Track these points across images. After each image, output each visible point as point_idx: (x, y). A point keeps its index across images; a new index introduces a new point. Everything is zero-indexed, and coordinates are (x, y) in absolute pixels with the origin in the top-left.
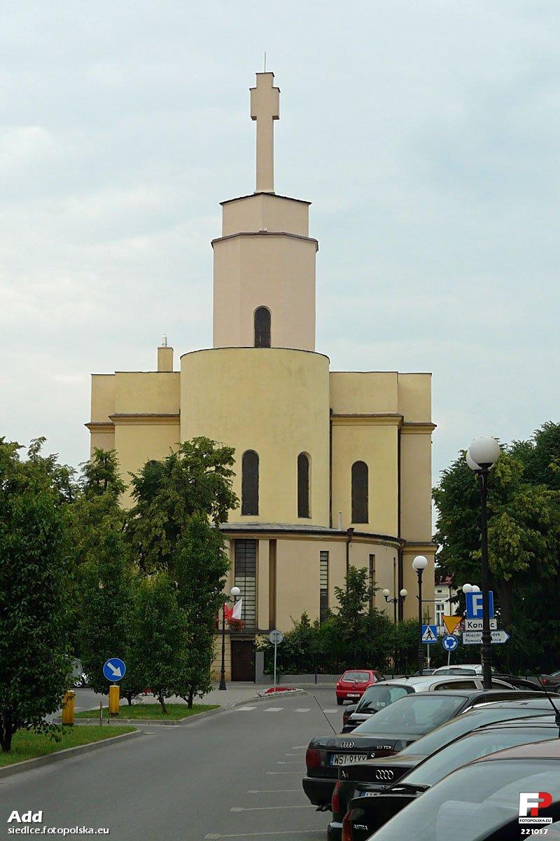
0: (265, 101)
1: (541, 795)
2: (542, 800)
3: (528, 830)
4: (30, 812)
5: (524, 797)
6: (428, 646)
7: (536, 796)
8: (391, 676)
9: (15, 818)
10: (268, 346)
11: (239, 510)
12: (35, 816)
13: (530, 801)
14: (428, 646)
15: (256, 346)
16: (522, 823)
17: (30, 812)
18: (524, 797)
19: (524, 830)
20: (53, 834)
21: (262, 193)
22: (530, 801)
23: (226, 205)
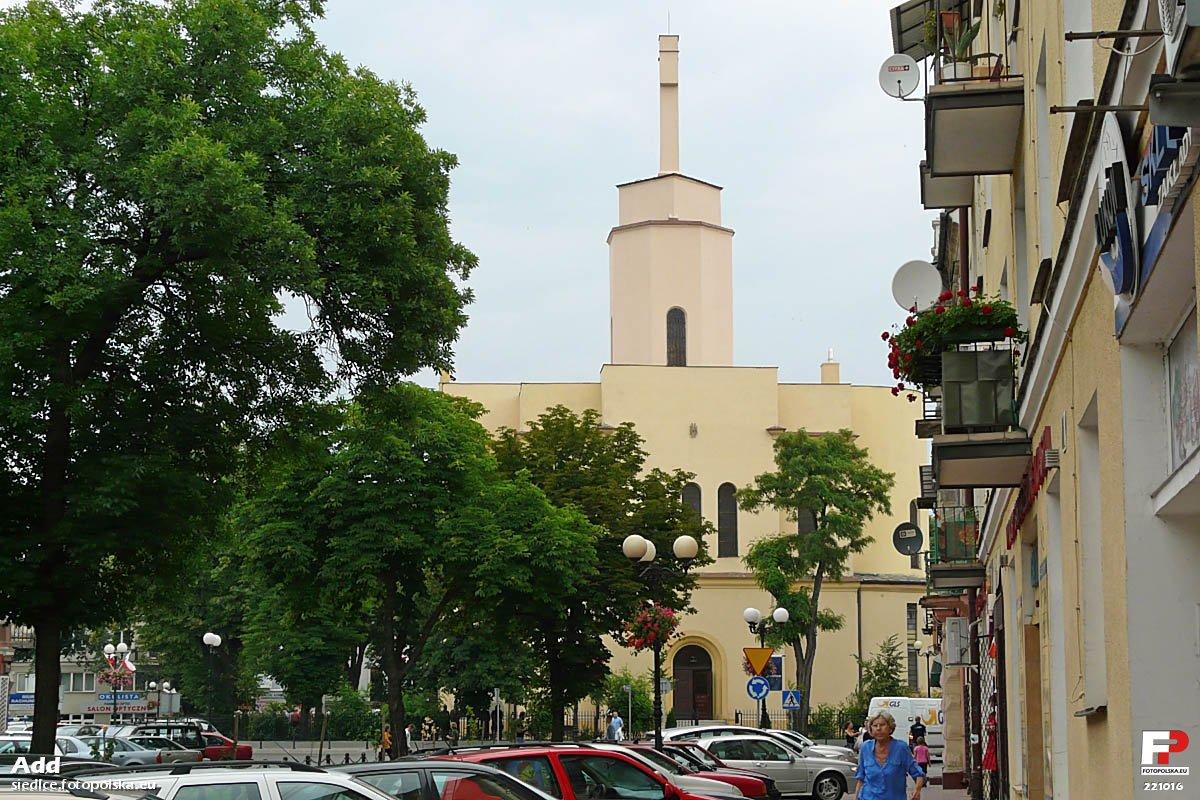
0: (669, 48)
1: (1173, 734)
2: (1175, 742)
3: (1155, 785)
4: (43, 759)
5: (1149, 737)
6: (1167, 128)
7: (1165, 735)
8: (824, 741)
9: (21, 767)
10: (685, 365)
11: (678, 630)
12: (50, 763)
13: (1157, 742)
14: (1167, 128)
15: (668, 365)
16: (1145, 773)
17: (43, 759)
18: (1149, 737)
19: (1148, 785)
20: (76, 789)
21: (673, 174)
22: (1157, 742)
23: (624, 189)
